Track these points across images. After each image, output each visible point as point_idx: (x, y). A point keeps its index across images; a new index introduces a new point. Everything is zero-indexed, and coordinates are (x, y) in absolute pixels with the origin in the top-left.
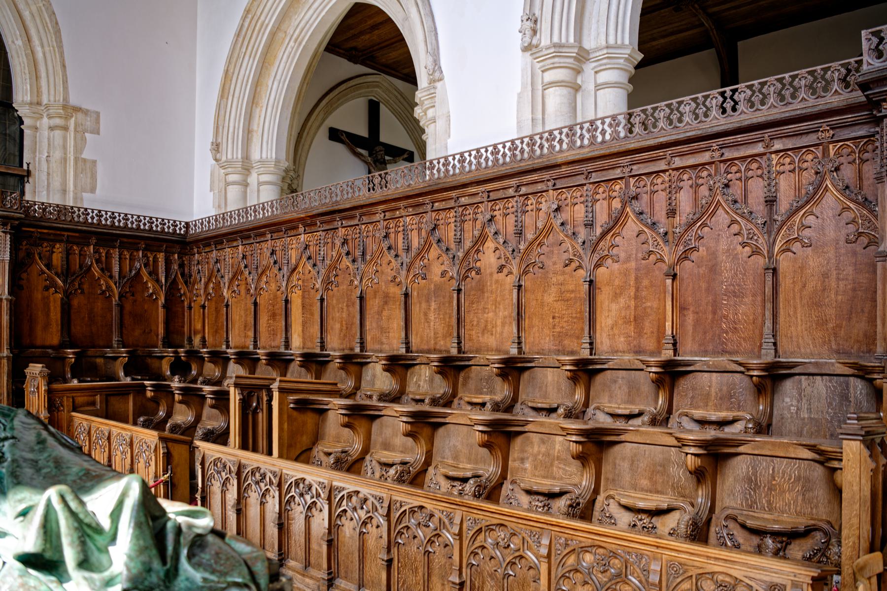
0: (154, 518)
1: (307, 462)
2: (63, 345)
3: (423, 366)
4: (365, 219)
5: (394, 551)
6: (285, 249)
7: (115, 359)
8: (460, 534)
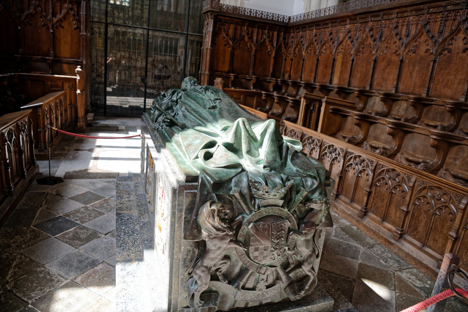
0: (279, 141)
1: (334, 137)
2: (229, 72)
3: (403, 101)
4: (385, 17)
5: (374, 189)
6: (337, 32)
7: (250, 80)
8: (413, 187)
